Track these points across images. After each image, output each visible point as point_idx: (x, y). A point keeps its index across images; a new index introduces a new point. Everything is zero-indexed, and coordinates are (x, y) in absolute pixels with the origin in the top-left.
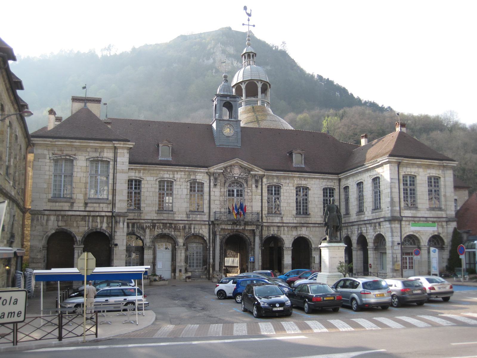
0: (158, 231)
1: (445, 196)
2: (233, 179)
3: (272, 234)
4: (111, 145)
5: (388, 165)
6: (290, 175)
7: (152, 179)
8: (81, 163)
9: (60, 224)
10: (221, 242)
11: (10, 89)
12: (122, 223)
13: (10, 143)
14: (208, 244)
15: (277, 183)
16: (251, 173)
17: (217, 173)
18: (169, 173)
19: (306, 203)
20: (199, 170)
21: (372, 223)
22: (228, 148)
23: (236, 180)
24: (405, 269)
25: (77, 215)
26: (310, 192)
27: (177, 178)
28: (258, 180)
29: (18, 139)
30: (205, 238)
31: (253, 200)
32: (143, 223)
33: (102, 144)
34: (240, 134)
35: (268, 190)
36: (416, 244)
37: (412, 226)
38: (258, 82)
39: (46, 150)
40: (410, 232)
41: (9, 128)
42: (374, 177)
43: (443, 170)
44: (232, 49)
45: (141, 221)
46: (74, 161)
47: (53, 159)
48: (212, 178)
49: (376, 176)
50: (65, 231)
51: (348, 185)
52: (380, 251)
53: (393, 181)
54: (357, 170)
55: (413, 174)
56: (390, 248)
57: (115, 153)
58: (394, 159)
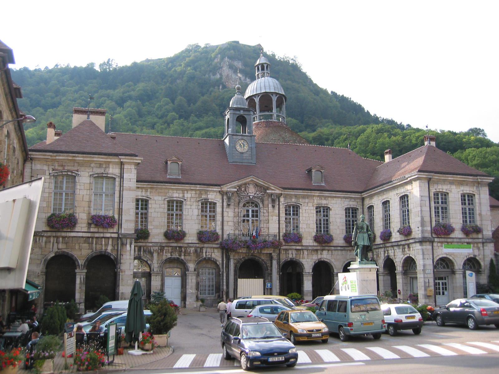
0: (166, 255)
1: (480, 215)
2: (248, 198)
3: (291, 258)
4: (117, 160)
5: (418, 182)
6: (309, 194)
7: (160, 198)
8: (84, 179)
9: (61, 246)
10: (235, 267)
11: (9, 94)
12: (129, 246)
13: (8, 155)
14: (221, 269)
15: (295, 203)
16: (268, 191)
17: (230, 191)
18: (178, 192)
19: (327, 224)
20: (211, 189)
21: (400, 245)
22: (242, 165)
23: (250, 199)
24: (438, 295)
25: (80, 237)
26: (331, 213)
27: (187, 198)
28: (275, 199)
29: (16, 152)
30: (218, 263)
31: (269, 221)
32: (150, 246)
33: (107, 158)
34: (254, 150)
35: (286, 210)
36: (450, 268)
37: (444, 248)
38: (272, 95)
39: (46, 165)
40: (442, 254)
41: (7, 138)
42: (402, 195)
43: (478, 187)
44: (240, 64)
45: (148, 244)
46: (76, 177)
47: (53, 176)
48: (225, 197)
49: (404, 194)
50: (66, 254)
51: (373, 205)
52: (410, 276)
53: (423, 198)
54: (383, 188)
55: (444, 191)
56: (422, 272)
57: (121, 169)
58: (424, 175)
